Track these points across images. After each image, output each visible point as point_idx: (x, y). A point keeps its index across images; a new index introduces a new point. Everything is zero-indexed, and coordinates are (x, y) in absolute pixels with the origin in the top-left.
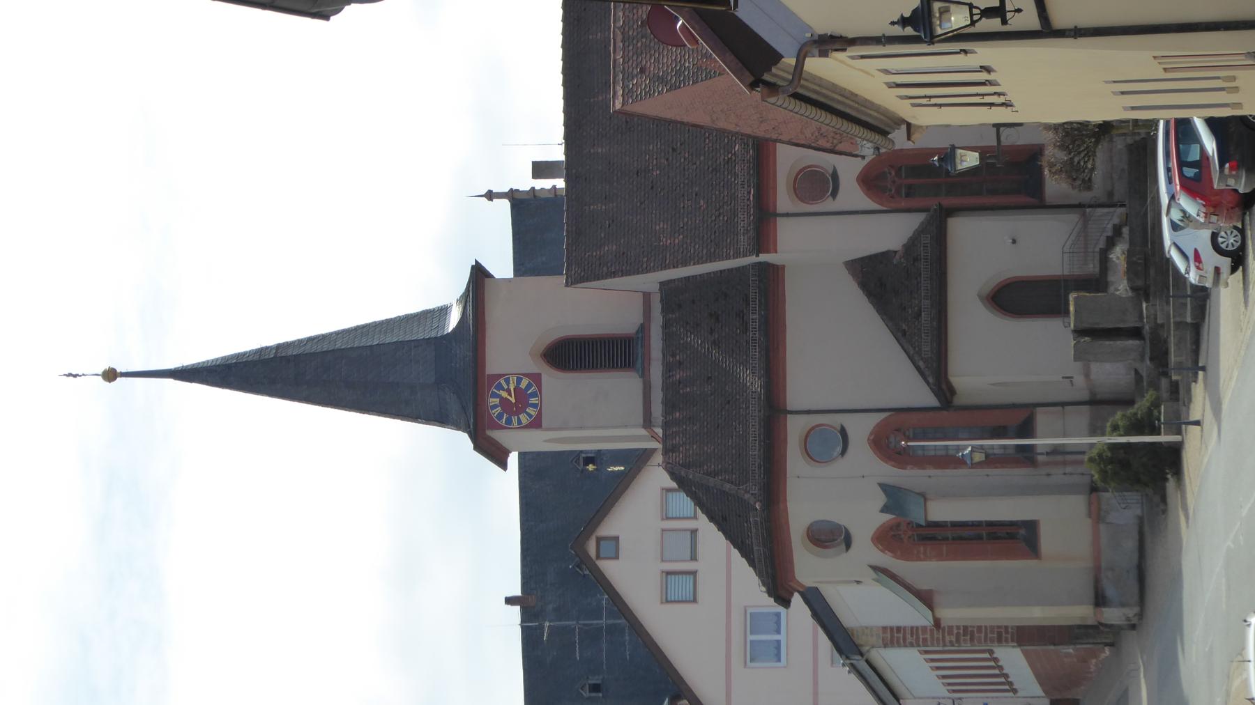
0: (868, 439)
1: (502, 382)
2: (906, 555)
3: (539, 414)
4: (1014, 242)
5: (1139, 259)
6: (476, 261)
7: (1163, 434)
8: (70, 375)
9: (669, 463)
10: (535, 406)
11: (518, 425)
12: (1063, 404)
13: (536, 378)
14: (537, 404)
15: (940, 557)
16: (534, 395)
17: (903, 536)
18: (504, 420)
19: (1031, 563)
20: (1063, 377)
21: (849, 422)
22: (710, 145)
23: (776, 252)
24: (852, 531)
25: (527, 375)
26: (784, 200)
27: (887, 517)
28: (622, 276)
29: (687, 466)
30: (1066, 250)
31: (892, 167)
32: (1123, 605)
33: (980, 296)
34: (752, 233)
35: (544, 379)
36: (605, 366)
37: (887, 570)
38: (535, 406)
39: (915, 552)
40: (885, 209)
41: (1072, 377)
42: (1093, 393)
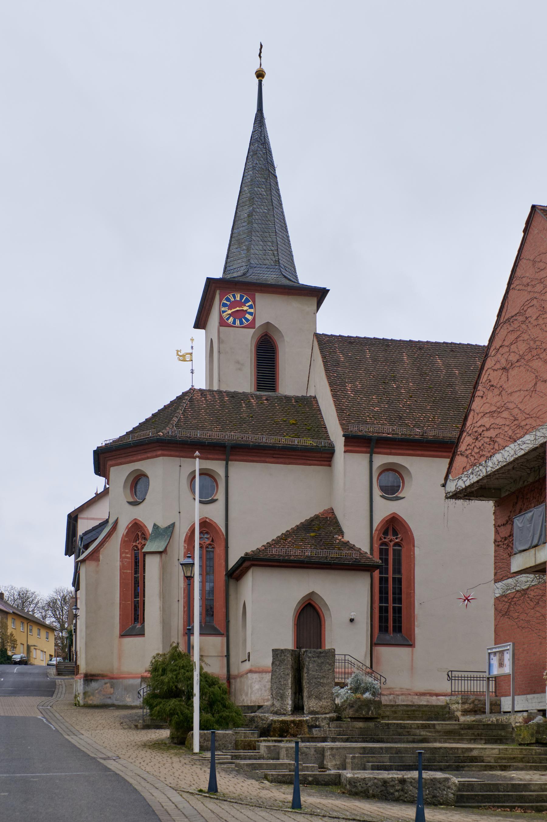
0: (206, 518)
1: (250, 303)
2: (125, 543)
3: (229, 326)
4: (352, 620)
5: (372, 712)
6: (329, 290)
7: (202, 731)
8: (261, 46)
9: (194, 392)
10: (234, 322)
11: (222, 311)
12: (228, 656)
13: (251, 325)
14: (235, 324)
15: (122, 568)
16: (241, 323)
17: (138, 542)
18: (226, 302)
19: (117, 631)
20: (249, 653)
21: (220, 505)
22: (417, 416)
23: (345, 452)
24: (141, 506)
25: (254, 319)
26: (380, 460)
27: (150, 529)
28: (323, 362)
29: (191, 400)
30: (347, 657)
31: (401, 540)
32: (85, 693)
33: (313, 593)
34: (360, 434)
35: (252, 331)
36: (258, 373)
37: (115, 530)
38: (234, 322)
39: (127, 551)
40: (374, 532)
41: (249, 660)
42: (235, 677)
